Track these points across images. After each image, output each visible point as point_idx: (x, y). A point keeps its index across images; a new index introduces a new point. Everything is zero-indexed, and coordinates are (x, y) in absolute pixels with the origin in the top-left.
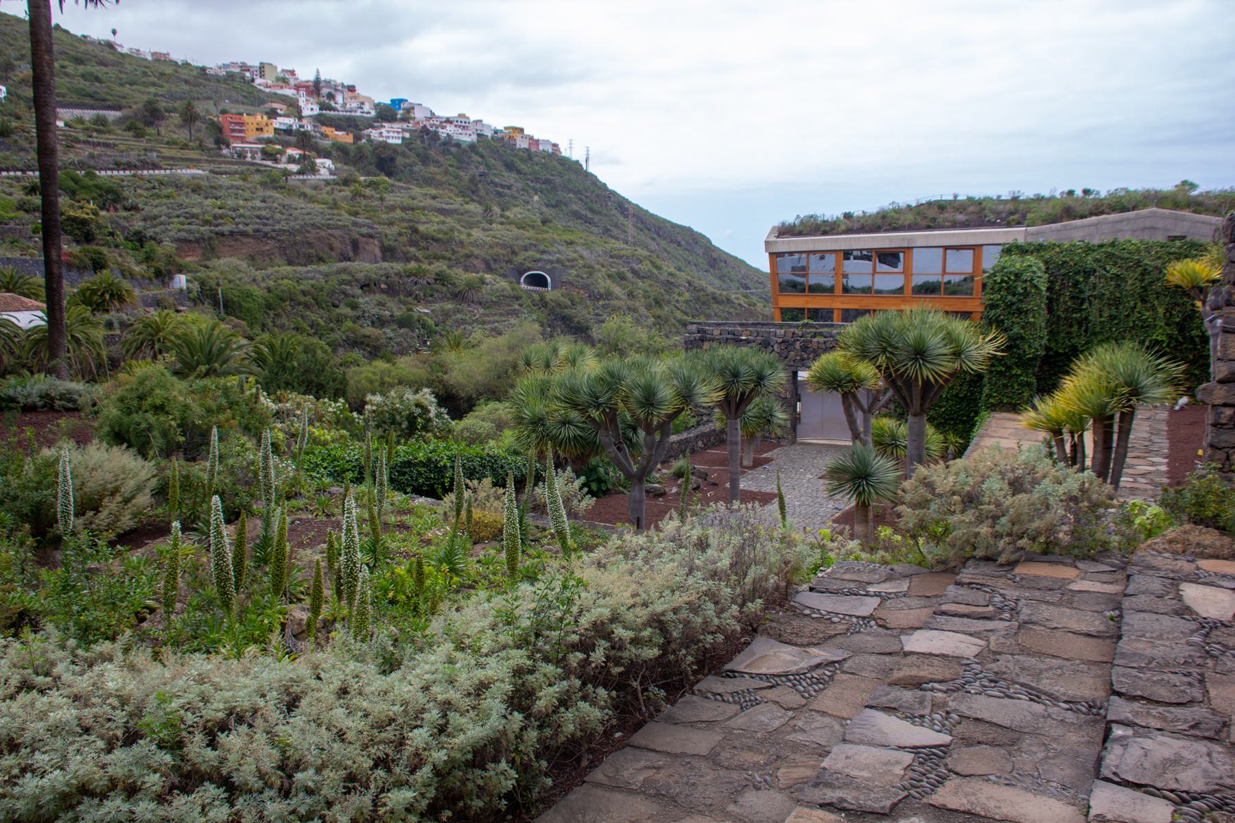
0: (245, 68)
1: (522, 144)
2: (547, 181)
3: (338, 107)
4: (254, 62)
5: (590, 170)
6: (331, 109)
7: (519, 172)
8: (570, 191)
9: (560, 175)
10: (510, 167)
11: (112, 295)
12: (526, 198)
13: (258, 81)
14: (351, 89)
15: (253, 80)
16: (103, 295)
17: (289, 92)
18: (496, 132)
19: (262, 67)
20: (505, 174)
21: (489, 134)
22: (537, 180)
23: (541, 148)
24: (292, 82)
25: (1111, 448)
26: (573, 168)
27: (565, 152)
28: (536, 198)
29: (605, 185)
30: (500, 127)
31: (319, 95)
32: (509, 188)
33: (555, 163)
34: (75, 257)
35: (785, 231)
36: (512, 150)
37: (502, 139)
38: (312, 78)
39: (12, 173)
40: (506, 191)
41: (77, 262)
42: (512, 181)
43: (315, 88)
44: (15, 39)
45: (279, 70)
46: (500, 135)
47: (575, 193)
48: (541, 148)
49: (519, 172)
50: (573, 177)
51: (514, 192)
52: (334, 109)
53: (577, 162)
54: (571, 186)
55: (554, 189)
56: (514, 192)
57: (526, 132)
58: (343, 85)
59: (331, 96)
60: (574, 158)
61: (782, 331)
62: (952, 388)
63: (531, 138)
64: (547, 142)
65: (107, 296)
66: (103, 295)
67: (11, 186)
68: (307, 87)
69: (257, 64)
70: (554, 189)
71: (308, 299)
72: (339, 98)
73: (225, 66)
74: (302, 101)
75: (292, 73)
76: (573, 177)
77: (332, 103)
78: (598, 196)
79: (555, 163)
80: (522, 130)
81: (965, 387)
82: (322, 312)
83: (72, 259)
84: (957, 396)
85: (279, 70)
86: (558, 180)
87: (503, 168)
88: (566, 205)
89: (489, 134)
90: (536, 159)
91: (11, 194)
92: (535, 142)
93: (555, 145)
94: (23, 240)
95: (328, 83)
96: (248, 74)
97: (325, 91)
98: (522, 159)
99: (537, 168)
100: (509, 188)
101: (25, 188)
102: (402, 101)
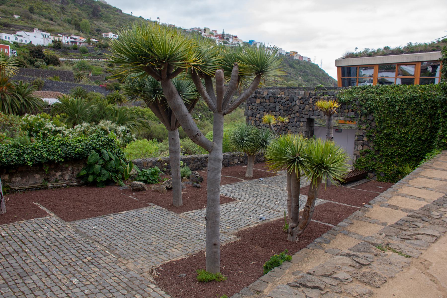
0: (199, 29)
1: (296, 58)
2: (304, 72)
3: (230, 43)
4: (202, 28)
5: (322, 68)
6: (227, 43)
7: (294, 68)
8: (313, 76)
9: (310, 69)
10: (291, 66)
11: (118, 100)
12: (297, 78)
13: (203, 34)
14: (236, 37)
15: (201, 33)
16: (114, 99)
17: (213, 38)
18: (287, 53)
19: (205, 29)
20: (289, 69)
21: (284, 54)
22: (301, 71)
23: (303, 59)
24: (215, 34)
25: (235, 179)
26: (316, 67)
27: (313, 61)
28: (300, 78)
29: (327, 74)
30: (289, 51)
31: (223, 38)
32: (290, 74)
33: (308, 65)
34: (109, 86)
35: (351, 56)
36: (292, 60)
37: (289, 56)
38: (221, 33)
39: (103, 60)
40: (289, 75)
41: (109, 87)
42: (291, 71)
43: (222, 36)
44: (126, 21)
45: (211, 30)
46: (288, 54)
47: (315, 77)
48: (303, 59)
49: (294, 68)
50: (315, 71)
51: (292, 75)
52: (228, 44)
53: (317, 65)
54: (314, 74)
55: (307, 75)
56: (292, 75)
57: (298, 54)
58: (233, 36)
59: (228, 39)
60: (316, 63)
61: (303, 92)
62: (416, 133)
63: (300, 56)
64: (306, 57)
65: (116, 100)
66: (114, 99)
67: (104, 64)
68: (220, 36)
69: (203, 28)
70: (307, 75)
71: (200, 107)
72: (231, 40)
73: (192, 29)
74: (217, 41)
75: (216, 31)
76: (315, 71)
77: (228, 41)
78: (324, 78)
79: (308, 65)
80: (297, 53)
81: (427, 132)
82: (204, 112)
83: (108, 87)
84: (420, 138)
85: (211, 30)
86: (309, 72)
87: (288, 67)
88: (311, 81)
89: (284, 54)
90: (301, 63)
91: (103, 67)
92: (301, 57)
93: (309, 59)
94: (102, 82)
95: (227, 35)
96: (200, 32)
97: (225, 37)
98: (296, 64)
99: (301, 67)
100: (290, 74)
101: (108, 65)
102: (253, 41)
